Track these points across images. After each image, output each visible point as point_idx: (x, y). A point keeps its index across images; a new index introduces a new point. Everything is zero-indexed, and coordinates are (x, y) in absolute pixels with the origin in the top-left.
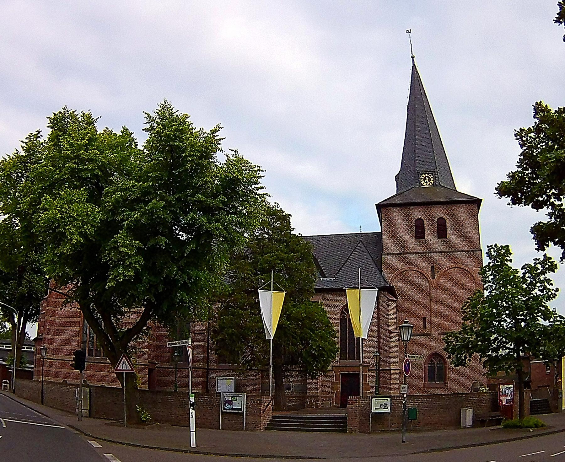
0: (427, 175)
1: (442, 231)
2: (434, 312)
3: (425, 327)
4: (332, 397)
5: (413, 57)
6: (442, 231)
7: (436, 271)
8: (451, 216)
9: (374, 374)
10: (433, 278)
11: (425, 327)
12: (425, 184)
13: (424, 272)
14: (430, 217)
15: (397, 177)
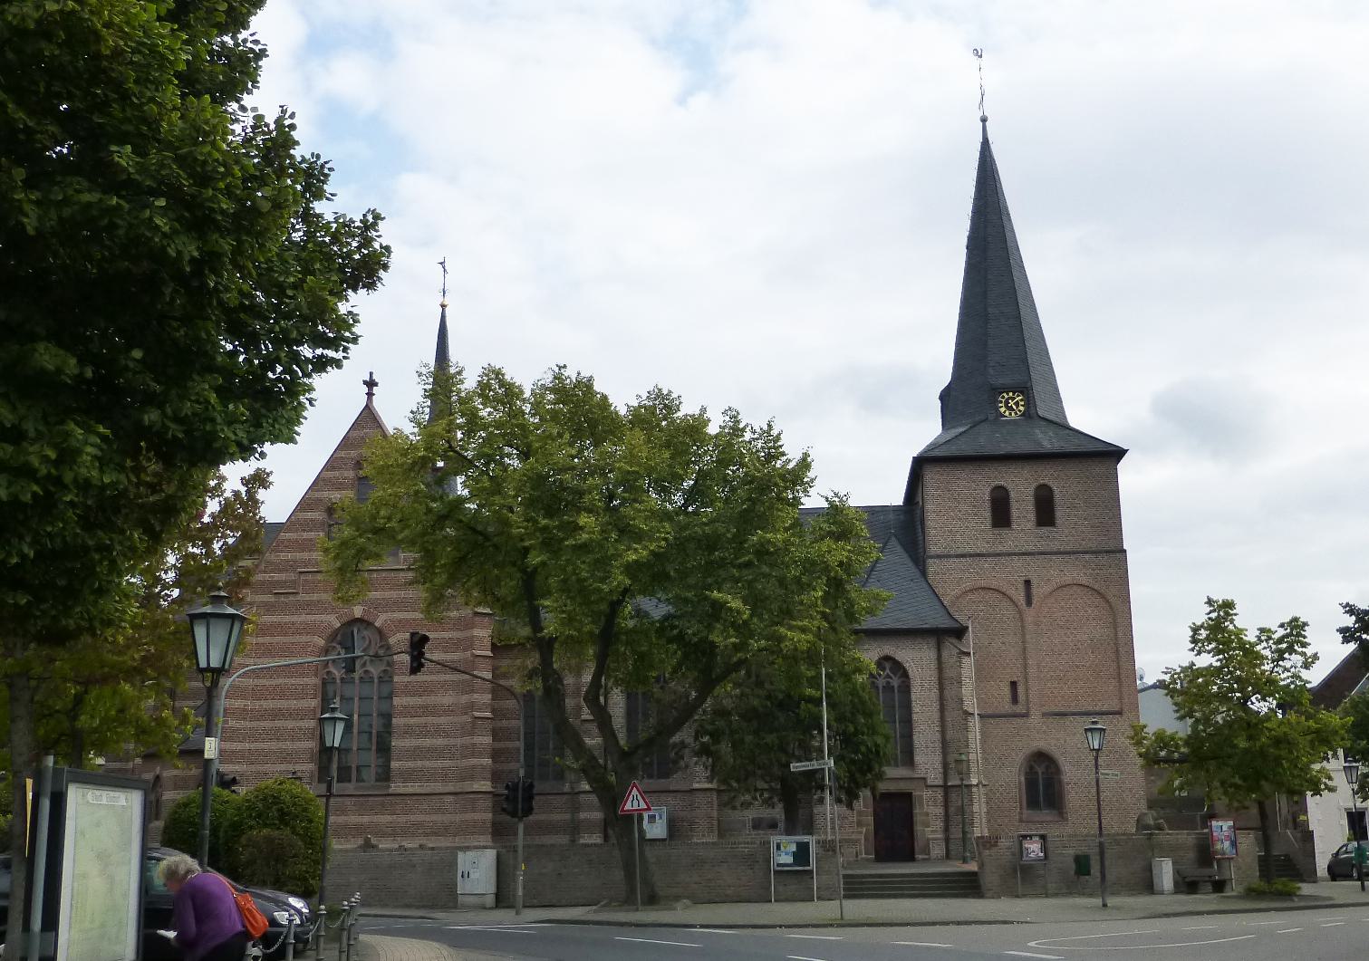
0: (1011, 394)
1: (1045, 511)
2: (1032, 671)
3: (1015, 700)
4: (857, 841)
5: (984, 120)
6: (1045, 511)
7: (1034, 591)
8: (1063, 483)
9: (940, 795)
10: (1029, 602)
11: (1015, 700)
12: (1007, 413)
13: (1011, 592)
14: (1021, 485)
15: (945, 396)
